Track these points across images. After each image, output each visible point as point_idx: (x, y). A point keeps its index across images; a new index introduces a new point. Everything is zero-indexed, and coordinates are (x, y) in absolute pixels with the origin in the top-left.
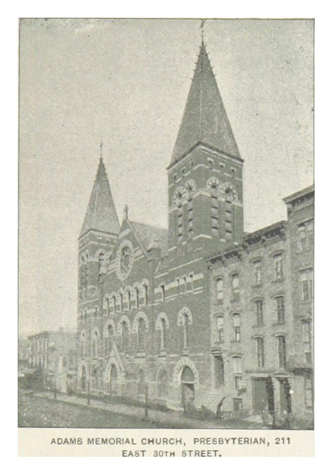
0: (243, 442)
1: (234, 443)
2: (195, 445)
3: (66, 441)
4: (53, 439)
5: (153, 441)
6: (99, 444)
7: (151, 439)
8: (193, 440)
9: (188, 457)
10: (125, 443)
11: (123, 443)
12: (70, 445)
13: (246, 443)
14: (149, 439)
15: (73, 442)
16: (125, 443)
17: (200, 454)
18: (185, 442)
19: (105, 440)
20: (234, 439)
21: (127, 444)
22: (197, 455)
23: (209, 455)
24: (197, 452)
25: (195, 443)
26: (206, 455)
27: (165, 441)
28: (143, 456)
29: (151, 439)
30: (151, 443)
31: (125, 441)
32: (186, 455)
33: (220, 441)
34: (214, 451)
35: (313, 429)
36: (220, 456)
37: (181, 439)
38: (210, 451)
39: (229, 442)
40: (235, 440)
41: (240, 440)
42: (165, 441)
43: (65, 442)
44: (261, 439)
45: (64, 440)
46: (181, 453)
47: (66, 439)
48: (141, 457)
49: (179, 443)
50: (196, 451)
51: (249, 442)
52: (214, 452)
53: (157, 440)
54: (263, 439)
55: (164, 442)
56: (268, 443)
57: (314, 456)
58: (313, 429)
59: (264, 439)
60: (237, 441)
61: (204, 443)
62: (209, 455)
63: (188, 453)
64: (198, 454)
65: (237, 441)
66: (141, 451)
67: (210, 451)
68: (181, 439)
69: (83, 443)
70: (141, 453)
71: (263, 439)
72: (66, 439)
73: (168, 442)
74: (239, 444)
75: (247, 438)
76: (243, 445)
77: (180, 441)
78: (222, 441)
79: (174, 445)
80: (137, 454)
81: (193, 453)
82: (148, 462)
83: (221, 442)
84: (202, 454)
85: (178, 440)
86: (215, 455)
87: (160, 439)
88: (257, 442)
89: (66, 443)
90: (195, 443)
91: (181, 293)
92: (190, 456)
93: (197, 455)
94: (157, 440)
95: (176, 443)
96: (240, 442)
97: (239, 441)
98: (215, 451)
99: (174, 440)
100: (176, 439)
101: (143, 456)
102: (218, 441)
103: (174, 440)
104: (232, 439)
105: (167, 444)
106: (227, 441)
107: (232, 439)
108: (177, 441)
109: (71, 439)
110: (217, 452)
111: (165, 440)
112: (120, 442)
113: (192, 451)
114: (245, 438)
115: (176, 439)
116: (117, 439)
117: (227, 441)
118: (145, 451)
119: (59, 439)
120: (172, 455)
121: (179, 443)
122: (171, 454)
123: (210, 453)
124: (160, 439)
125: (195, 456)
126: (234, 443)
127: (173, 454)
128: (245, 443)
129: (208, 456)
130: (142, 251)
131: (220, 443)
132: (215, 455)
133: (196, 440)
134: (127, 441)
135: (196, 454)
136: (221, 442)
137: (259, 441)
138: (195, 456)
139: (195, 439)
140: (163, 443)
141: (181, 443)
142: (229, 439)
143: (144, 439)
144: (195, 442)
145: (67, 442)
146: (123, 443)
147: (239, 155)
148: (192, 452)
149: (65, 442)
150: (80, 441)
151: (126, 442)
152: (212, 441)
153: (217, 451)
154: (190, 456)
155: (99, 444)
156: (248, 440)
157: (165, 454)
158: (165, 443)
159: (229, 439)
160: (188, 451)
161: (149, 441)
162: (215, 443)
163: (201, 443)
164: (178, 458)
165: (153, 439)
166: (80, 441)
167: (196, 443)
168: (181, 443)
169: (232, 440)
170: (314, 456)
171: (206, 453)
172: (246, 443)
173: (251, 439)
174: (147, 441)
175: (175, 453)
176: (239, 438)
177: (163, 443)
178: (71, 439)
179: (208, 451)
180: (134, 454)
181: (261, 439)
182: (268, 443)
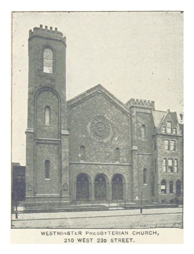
0: (115, 234)
2: (86, 235)
5: (92, 233)
7: (138, 232)
11: (120, 234)
13: (117, 234)
14: (137, 232)
17: (122, 240)
21: (123, 234)
23: (127, 241)
25: (86, 234)
26: (125, 241)
28: (91, 241)
30: (138, 234)
31: (121, 233)
32: (113, 241)
33: (101, 233)
34: (130, 239)
36: (134, 242)
37: (156, 232)
38: (128, 239)
39: (106, 234)
40: (56, 233)
46: (111, 240)
49: (155, 234)
50: (119, 239)
51: (119, 233)
52: (130, 240)
53: (141, 232)
54: (127, 232)
55: (146, 233)
56: (158, 234)
57: (182, 242)
59: (128, 232)
61: (118, 234)
62: (127, 241)
63: (114, 240)
64: (120, 240)
67: (128, 239)
70: (90, 240)
71: (127, 232)
73: (148, 233)
76: (115, 235)
77: (156, 233)
78: (103, 233)
81: (117, 240)
87: (144, 232)
88: (123, 234)
90: (86, 234)
92: (116, 242)
93: (120, 241)
94: (141, 232)
95: (137, 234)
96: (113, 234)
98: (131, 239)
99: (152, 232)
100: (153, 232)
101: (91, 241)
102: (100, 233)
103: (152, 232)
105: (148, 234)
108: (154, 233)
110: (92, 240)
111: (147, 232)
112: (118, 233)
115: (153, 232)
118: (132, 239)
121: (155, 234)
124: (144, 232)
125: (119, 242)
130: (166, 187)
132: (131, 241)
134: (123, 233)
135: (119, 241)
136: (102, 234)
137: (124, 233)
140: (146, 234)
141: (156, 234)
143: (134, 231)
144: (86, 233)
146: (62, 234)
147: (19, 206)
151: (122, 234)
152: (115, 233)
153: (92, 239)
156: (118, 232)
158: (147, 234)
163: (90, 234)
164: (108, 245)
167: (87, 234)
168: (156, 234)
170: (182, 242)
171: (125, 240)
172: (117, 234)
173: (120, 232)
174: (152, 233)
177: (146, 234)
179: (127, 239)
181: (126, 232)
182: (158, 234)
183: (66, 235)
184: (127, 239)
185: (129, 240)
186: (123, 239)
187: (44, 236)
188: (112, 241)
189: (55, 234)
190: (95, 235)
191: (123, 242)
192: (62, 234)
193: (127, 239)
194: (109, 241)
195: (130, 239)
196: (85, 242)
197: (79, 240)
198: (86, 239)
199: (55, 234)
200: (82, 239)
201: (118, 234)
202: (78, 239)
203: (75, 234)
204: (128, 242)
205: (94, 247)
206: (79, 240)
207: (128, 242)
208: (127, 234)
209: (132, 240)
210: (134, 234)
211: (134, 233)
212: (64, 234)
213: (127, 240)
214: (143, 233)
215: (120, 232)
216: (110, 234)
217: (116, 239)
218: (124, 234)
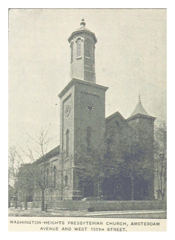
1: (87, 224)
3: (154, 224)
4: (132, 223)
6: (91, 224)
7: (57, 223)
8: (68, 222)
9: (110, 232)
10: (97, 224)
11: (96, 224)
12: (134, 225)
13: (148, 225)
14: (110, 223)
15: (136, 224)
16: (14, 223)
17: (116, 230)
18: (127, 224)
19: (136, 223)
20: (87, 222)
21: (98, 224)
22: (115, 230)
24: (115, 229)
25: (68, 224)
26: (119, 230)
27: (118, 224)
28: (86, 230)
29: (22, 221)
30: (111, 224)
31: (97, 223)
33: (80, 223)
34: (123, 228)
35: (166, 218)
36: (126, 231)
37: (126, 223)
38: (122, 228)
39: (85, 224)
40: (88, 223)
41: (145, 223)
42: (118, 224)
43: (154, 224)
44: (101, 222)
45: (153, 223)
46: (107, 229)
47: (154, 223)
48: (122, 232)
50: (114, 228)
52: (123, 229)
53: (114, 223)
55: (117, 224)
56: (127, 225)
58: (166, 218)
59: (102, 222)
60: (89, 223)
61: (94, 224)
63: (110, 229)
65: (89, 223)
66: (111, 228)
67: (122, 228)
68: (126, 223)
69: (65, 223)
70: (85, 229)
72: (154, 223)
73: (119, 224)
74: (145, 225)
75: (118, 222)
76: (147, 226)
77: (125, 224)
78: (82, 223)
79: (19, 224)
80: (83, 230)
81: (113, 229)
82: (73, 234)
83: (81, 224)
84: (117, 230)
85: (22, 223)
86: (124, 231)
87: (116, 223)
89: (154, 225)
90: (68, 224)
91: (109, 131)
92: (112, 230)
93: (115, 230)
94: (114, 223)
97: (145, 224)
98: (124, 229)
101: (86, 230)
102: (80, 223)
104: (86, 222)
105: (119, 225)
106: (84, 223)
107: (86, 222)
108: (124, 224)
109: (135, 223)
113: (112, 228)
114: (148, 223)
116: (117, 222)
117: (84, 223)
119: (151, 223)
120: (103, 230)
121: (125, 224)
122: (102, 229)
123: (121, 230)
125: (114, 231)
126: (87, 224)
127: (57, 229)
128: (148, 225)
129: (120, 231)
131: (80, 224)
132: (124, 231)
133: (69, 222)
134: (98, 223)
135: (114, 230)
136: (81, 224)
138: (114, 231)
139: (69, 222)
141: (126, 225)
142: (85, 222)
144: (69, 223)
145: (155, 224)
146: (24, 223)
148: (112, 229)
149: (154, 224)
150: (139, 224)
151: (98, 224)
154: (112, 230)
155: (91, 224)
157: (99, 230)
159: (85, 222)
160: (85, 228)
161: (110, 223)
162: (18, 223)
163: (71, 224)
164: (106, 232)
165: (47, 222)
166: (139, 224)
167: (69, 224)
168: (126, 225)
169: (86, 223)
172: (148, 225)
173: (96, 222)
175: (104, 229)
176: (145, 223)
178: (135, 223)
179: (120, 228)
180: (17, 222)
181: (101, 222)
182: (127, 225)
183: (27, 224)
184: (121, 229)
185: (123, 230)
186: (117, 228)
187: (12, 224)
188: (108, 230)
189: (142, 225)
190: (76, 224)
191: (117, 231)
192: (24, 223)
193: (121, 229)
194: (106, 229)
195: (123, 228)
196: (80, 230)
197: (76, 229)
198: (96, 230)
199: (142, 225)
200: (13, 221)
201: (94, 224)
202: (10, 221)
203: (144, 224)
204: (121, 231)
205: (89, 234)
206: (76, 229)
207: (121, 231)
208: (102, 224)
209: (125, 229)
210: (121, 224)
211: (108, 224)
212: (25, 223)
213: (120, 230)
214: (115, 224)
215: (96, 222)
216: (34, 223)
217: (112, 228)
218: (155, 225)
